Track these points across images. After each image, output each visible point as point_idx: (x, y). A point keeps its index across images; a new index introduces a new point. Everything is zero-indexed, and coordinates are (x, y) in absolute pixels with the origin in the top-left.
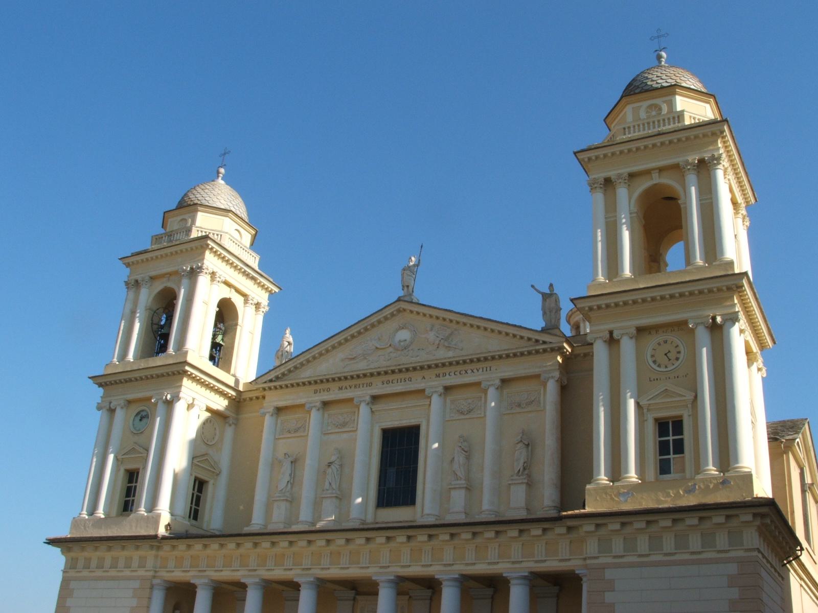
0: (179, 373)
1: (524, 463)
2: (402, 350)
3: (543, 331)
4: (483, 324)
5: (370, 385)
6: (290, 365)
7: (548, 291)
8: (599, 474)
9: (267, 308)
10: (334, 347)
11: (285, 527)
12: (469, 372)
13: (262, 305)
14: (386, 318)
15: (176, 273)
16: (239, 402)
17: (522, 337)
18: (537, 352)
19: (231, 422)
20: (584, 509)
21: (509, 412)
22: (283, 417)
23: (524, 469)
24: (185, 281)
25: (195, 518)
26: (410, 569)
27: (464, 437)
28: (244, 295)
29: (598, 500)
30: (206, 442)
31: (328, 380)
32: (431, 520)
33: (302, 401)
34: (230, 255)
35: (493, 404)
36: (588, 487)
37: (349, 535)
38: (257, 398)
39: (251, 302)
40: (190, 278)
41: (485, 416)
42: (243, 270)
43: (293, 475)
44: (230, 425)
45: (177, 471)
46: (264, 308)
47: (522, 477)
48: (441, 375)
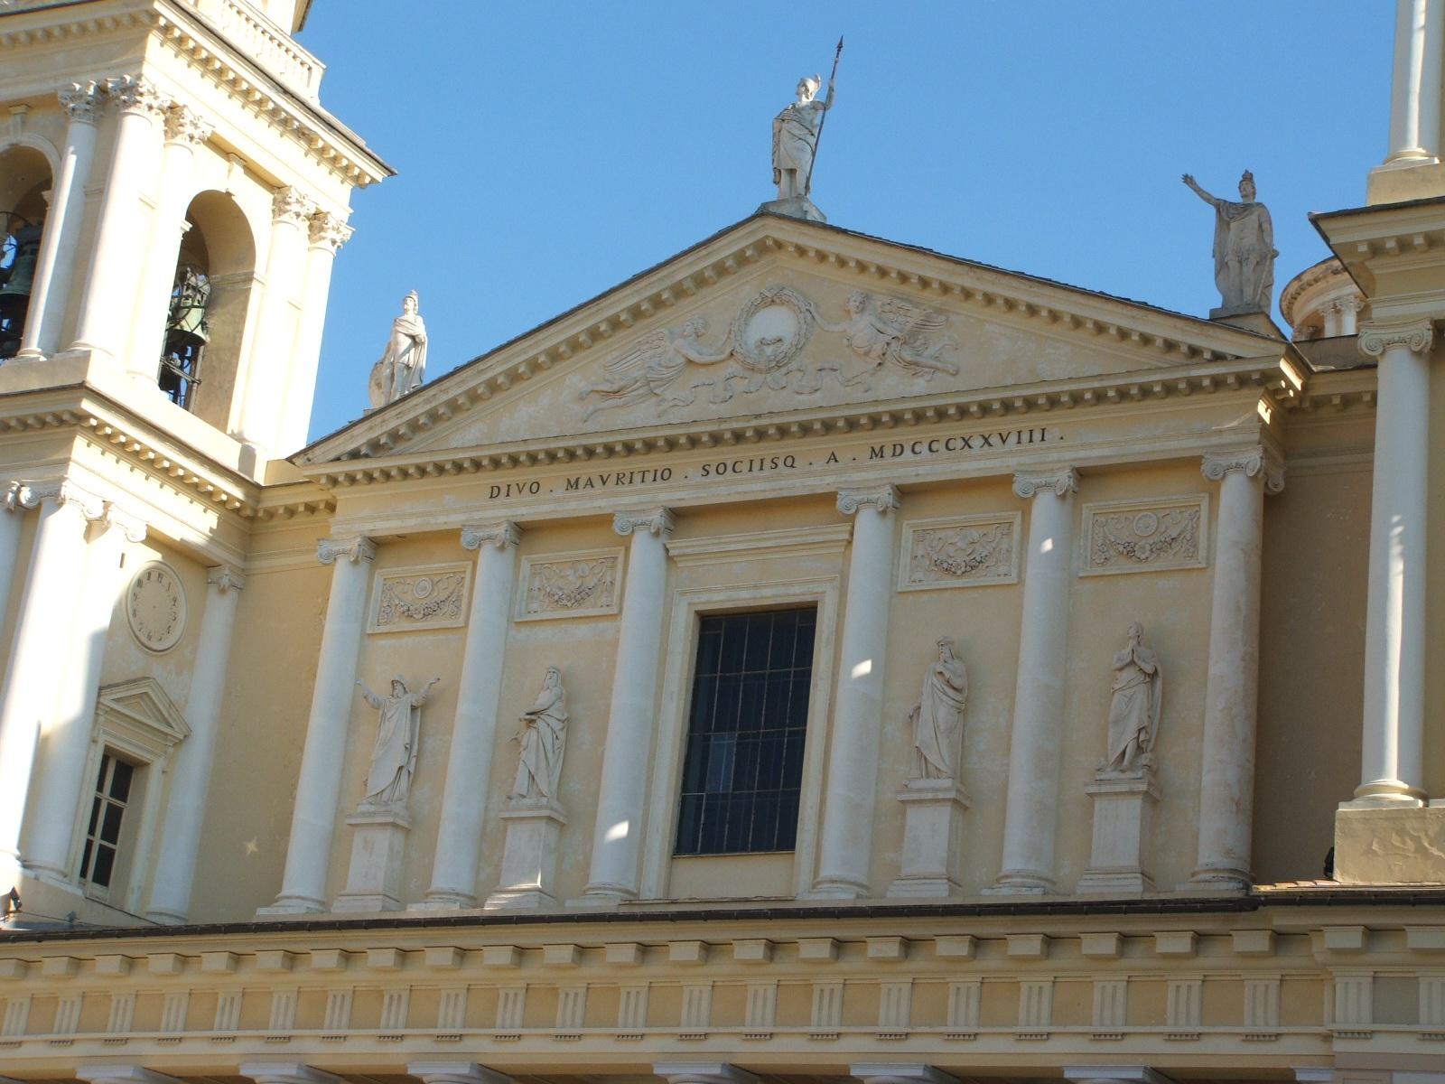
0: (61, 422)
1: (1140, 731)
2: (769, 370)
3: (1217, 320)
4: (1023, 294)
5: (665, 475)
6: (417, 408)
7: (1235, 197)
8: (1380, 770)
9: (347, 232)
10: (555, 356)
11: (384, 909)
12: (977, 442)
13: (331, 222)
14: (721, 270)
15: (49, 102)
16: (252, 519)
17: (1146, 340)
18: (1194, 386)
19: (225, 581)
20: (1331, 879)
21: (1099, 571)
22: (392, 569)
23: (1140, 749)
24: (80, 131)
25: (102, 877)
26: (524, 1047)
27: (952, 643)
28: (274, 186)
29: (1375, 853)
30: (144, 640)
31: (533, 458)
32: (843, 897)
33: (452, 520)
34: (203, 34)
35: (1048, 545)
36: (1344, 809)
37: (587, 935)
38: (311, 509)
39: (295, 208)
40: (97, 123)
41: (1021, 581)
42: (271, 106)
43: (416, 749)
44: (223, 591)
45: (45, 730)
46: (338, 230)
47: (1129, 775)
48: (888, 452)
